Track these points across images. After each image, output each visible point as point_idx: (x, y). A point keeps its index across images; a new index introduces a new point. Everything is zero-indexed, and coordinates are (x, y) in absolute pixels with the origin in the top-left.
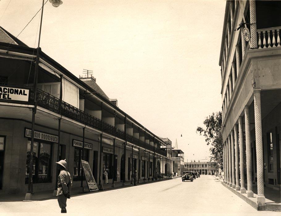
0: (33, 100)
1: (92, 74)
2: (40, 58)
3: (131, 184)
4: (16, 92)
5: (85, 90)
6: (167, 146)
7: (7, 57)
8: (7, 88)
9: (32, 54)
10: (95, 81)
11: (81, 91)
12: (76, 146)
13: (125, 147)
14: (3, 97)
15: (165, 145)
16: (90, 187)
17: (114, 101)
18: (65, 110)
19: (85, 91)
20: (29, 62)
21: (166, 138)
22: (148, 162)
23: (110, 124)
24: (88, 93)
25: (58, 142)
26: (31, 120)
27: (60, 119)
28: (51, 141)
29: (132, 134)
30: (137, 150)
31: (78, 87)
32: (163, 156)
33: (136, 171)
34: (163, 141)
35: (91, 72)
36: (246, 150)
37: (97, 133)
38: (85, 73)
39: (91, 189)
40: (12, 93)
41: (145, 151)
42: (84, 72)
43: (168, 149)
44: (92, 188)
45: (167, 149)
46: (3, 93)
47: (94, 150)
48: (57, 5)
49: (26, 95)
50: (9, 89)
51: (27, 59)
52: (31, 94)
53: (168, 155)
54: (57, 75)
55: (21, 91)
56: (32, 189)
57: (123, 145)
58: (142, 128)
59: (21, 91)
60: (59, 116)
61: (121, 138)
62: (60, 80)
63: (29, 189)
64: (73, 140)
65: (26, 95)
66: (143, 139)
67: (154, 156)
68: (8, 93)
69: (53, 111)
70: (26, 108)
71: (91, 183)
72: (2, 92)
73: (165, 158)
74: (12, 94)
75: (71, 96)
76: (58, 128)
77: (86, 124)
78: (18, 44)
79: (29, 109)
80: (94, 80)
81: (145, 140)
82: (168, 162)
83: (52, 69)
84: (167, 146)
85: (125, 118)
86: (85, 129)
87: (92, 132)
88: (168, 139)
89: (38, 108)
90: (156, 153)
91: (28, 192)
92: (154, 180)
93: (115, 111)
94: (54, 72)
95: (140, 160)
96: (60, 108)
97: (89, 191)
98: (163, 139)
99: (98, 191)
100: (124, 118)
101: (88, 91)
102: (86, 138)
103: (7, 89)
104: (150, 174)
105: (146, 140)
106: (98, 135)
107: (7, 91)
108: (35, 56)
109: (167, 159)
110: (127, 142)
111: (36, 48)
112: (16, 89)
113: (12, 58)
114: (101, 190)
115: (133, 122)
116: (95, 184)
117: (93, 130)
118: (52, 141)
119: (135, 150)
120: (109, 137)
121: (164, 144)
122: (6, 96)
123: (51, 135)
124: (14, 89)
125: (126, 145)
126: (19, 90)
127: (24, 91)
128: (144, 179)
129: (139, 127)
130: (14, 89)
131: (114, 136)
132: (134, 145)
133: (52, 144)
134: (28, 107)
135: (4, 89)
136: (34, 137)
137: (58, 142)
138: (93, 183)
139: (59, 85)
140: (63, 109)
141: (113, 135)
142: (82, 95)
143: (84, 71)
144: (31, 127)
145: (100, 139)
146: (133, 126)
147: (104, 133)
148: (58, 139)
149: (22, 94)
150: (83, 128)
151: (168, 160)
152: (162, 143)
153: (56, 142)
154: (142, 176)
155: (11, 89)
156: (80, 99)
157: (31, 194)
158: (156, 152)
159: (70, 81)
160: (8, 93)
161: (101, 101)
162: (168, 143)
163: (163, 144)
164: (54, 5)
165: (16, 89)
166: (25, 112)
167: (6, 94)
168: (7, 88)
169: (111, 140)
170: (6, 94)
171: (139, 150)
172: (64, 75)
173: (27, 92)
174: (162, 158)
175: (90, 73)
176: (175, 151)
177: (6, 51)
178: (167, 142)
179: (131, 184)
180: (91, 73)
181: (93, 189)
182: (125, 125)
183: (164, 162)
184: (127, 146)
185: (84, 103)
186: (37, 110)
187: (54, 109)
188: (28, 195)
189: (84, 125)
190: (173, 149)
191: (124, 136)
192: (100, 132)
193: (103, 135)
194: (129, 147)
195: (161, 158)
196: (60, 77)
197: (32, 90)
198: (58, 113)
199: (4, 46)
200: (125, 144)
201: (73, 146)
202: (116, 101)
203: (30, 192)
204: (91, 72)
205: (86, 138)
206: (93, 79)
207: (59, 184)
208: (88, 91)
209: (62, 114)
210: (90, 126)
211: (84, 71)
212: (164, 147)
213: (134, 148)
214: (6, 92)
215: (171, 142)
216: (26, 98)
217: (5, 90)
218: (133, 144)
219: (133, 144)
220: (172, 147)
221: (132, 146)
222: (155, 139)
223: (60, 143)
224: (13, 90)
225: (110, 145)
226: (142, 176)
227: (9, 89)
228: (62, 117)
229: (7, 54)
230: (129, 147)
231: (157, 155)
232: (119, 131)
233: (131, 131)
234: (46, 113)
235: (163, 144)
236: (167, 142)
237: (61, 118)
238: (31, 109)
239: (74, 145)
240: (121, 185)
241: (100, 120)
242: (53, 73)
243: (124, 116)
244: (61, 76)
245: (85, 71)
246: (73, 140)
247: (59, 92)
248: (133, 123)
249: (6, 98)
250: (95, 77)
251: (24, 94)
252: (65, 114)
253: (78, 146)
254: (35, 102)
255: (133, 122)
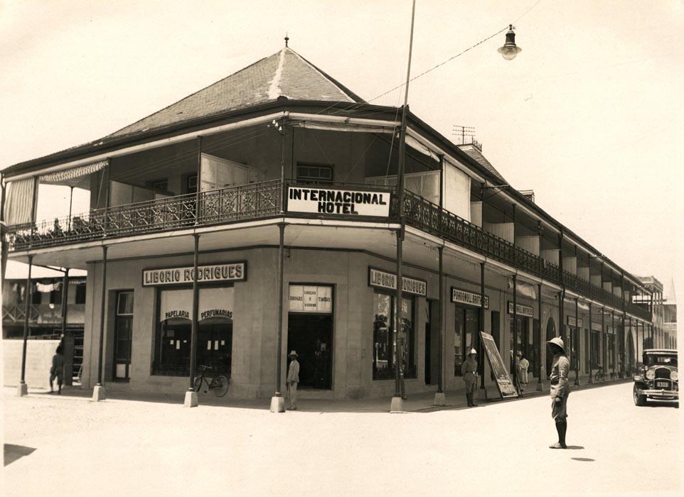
0: (398, 214)
1: (473, 134)
2: (408, 127)
3: (575, 384)
4: (367, 199)
5: (483, 180)
6: (652, 297)
7: (345, 130)
8: (351, 192)
9: (393, 120)
10: (481, 150)
11: (473, 181)
12: (458, 301)
13: (561, 302)
14: (344, 211)
15: (648, 294)
16: (502, 390)
17: (527, 196)
18: (456, 232)
19: (483, 184)
20: (389, 136)
21: (650, 276)
22: (586, 330)
23: (530, 251)
24: (490, 187)
25: (424, 294)
26: (394, 254)
27: (441, 249)
28: (412, 292)
29: (575, 272)
30: (586, 307)
31: (469, 176)
32: (643, 320)
33: (474, 351)
34: (643, 285)
35: (471, 130)
36: (286, 98)
37: (506, 273)
38: (457, 133)
39: (505, 394)
40: (359, 202)
41: (603, 309)
42: (455, 132)
43: (654, 303)
44: (506, 391)
45: (651, 304)
46: (343, 202)
47: (491, 309)
48: (511, 56)
49: (385, 203)
50: (353, 194)
51: (381, 131)
52: (394, 200)
53: (654, 317)
54: (434, 157)
55: (375, 196)
56: (403, 392)
57: (556, 297)
58: (595, 256)
59: (375, 196)
60: (439, 241)
61: (553, 282)
62: (438, 166)
63: (397, 390)
64: (452, 288)
65: (385, 203)
66: (597, 281)
67: (623, 320)
68: (353, 202)
69: (430, 233)
70: (383, 230)
71: (503, 381)
72: (341, 201)
73: (648, 325)
74: (358, 204)
75: (455, 197)
76: (395, 256)
77: (487, 254)
78: (354, 102)
79: (390, 232)
80: (478, 148)
81: (602, 284)
82: (656, 334)
83: (423, 144)
84: (652, 297)
85: (560, 237)
86: (485, 266)
87: (497, 271)
88: (655, 280)
89: (407, 228)
90: (627, 314)
91: (396, 396)
92: (625, 377)
93: (539, 221)
94: (429, 149)
95: (565, 326)
96: (441, 225)
97: (501, 398)
98: (641, 278)
99: (517, 398)
100: (558, 235)
101: (489, 184)
102: (488, 287)
103: (349, 195)
104: (611, 363)
105: (615, 289)
106: (507, 277)
107: (350, 198)
108: (398, 124)
109: (652, 327)
110: (567, 291)
111: (400, 106)
112: (367, 193)
113: (355, 130)
114: (520, 397)
115: (576, 244)
116: (509, 384)
117: (499, 267)
118: (415, 292)
119: (582, 310)
120: (528, 281)
121: (644, 290)
122: (349, 209)
123: (413, 280)
124: (362, 193)
125: (564, 297)
126: (372, 194)
127: (381, 196)
128: (612, 375)
129: (589, 255)
130: (362, 193)
131: (538, 276)
132: (580, 297)
133: (413, 298)
134: (389, 229)
135: (345, 194)
136: (403, 290)
137: (424, 294)
138: (505, 381)
139: (438, 177)
140: (446, 226)
141: (538, 276)
142: (477, 193)
143: (455, 128)
144: (395, 270)
145: (512, 286)
146: (574, 251)
147: (519, 273)
148: (425, 287)
149: (377, 203)
150: (481, 264)
151: (656, 330)
152: (639, 288)
153: (422, 294)
154: (610, 367)
155: (358, 194)
156: (471, 201)
157: (402, 398)
158: (629, 312)
159: (456, 165)
160: (353, 202)
161: (513, 201)
162: (655, 289)
163: (642, 291)
164: (505, 56)
165: (367, 193)
166: (380, 238)
167: (349, 205)
168: (351, 192)
169: (532, 288)
170: (349, 205)
171: (590, 307)
172: (447, 156)
173: (386, 197)
174: (641, 325)
175: (468, 133)
176: (669, 307)
177: (345, 118)
178: (652, 285)
179: (575, 384)
180: (470, 133)
181: (508, 394)
182: (560, 252)
183: (640, 334)
184: (565, 300)
185: (481, 209)
186: (406, 234)
187: (422, 223)
188: (396, 401)
189: (482, 258)
190: (664, 303)
191: (557, 275)
192: (513, 270)
193: (517, 278)
194: (568, 301)
195: (639, 324)
196: (439, 160)
197: (394, 193)
198: (438, 236)
199: (343, 108)
200: (561, 295)
201: (451, 301)
202: (531, 196)
203: (399, 396)
204: (471, 130)
205: (488, 287)
206: (476, 147)
207: (554, 377)
208: (489, 184)
209: (445, 238)
210: (494, 258)
211: (455, 128)
212: (645, 298)
213: (579, 305)
214: (349, 200)
215: (662, 285)
216: (384, 211)
217: (348, 197)
218: (577, 295)
219: (577, 295)
220: (664, 298)
221: (576, 299)
222: (625, 280)
223: (428, 296)
224: (360, 195)
225: (530, 298)
226: (610, 367)
227: (353, 194)
228: (446, 245)
229: (346, 124)
230: (568, 301)
231: (630, 318)
232: (549, 265)
233: (571, 265)
234: (419, 239)
235: (642, 291)
236: (652, 285)
237: (443, 246)
238: (395, 232)
239: (455, 300)
240: (534, 390)
241: (512, 245)
242: (427, 153)
243: (558, 231)
244: (440, 156)
245: (458, 128)
246: (452, 288)
247: (437, 193)
248: (576, 246)
249: (349, 212)
250: (480, 142)
251: (382, 203)
252: (449, 236)
253: (462, 302)
254: (401, 218)
255: (576, 244)
